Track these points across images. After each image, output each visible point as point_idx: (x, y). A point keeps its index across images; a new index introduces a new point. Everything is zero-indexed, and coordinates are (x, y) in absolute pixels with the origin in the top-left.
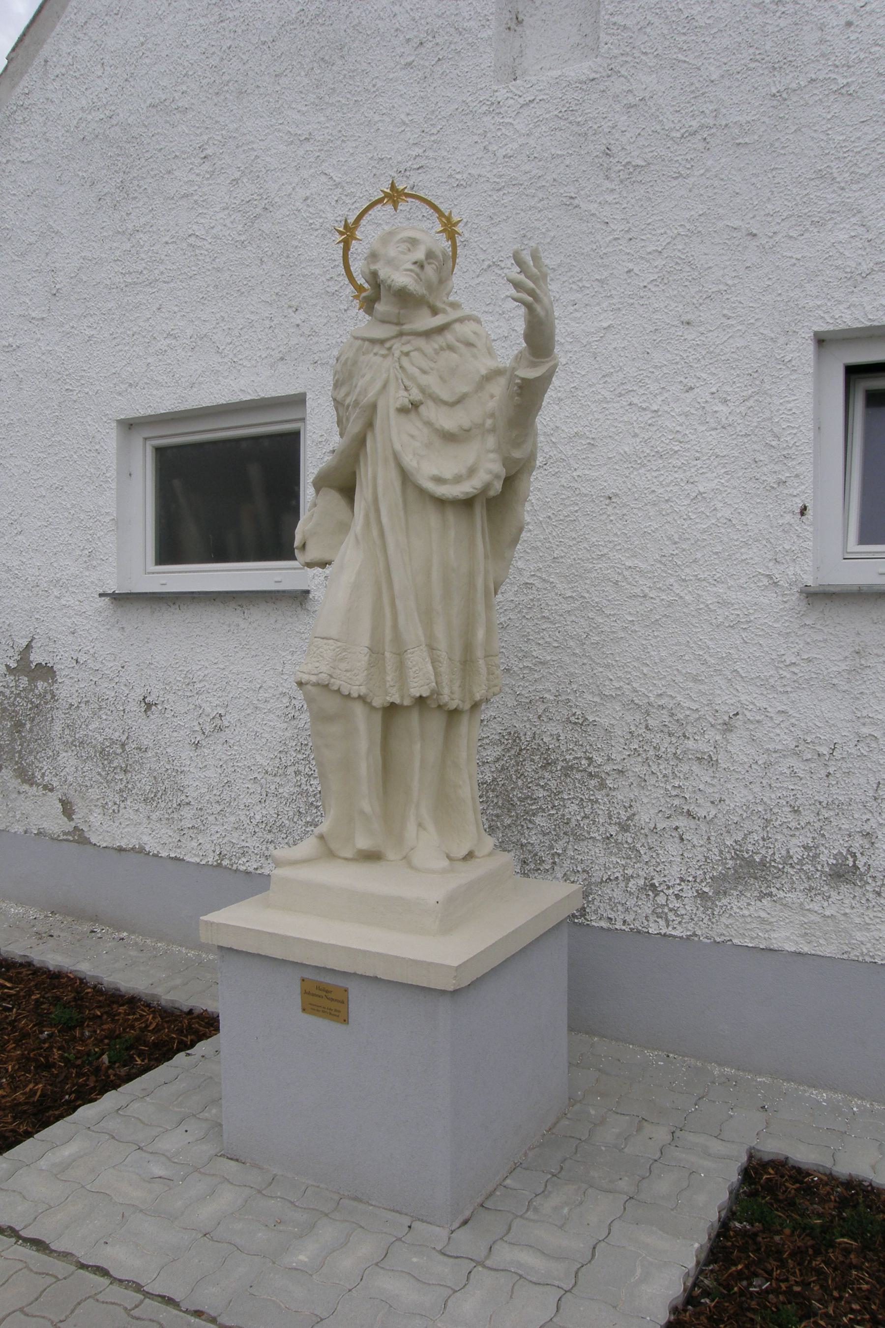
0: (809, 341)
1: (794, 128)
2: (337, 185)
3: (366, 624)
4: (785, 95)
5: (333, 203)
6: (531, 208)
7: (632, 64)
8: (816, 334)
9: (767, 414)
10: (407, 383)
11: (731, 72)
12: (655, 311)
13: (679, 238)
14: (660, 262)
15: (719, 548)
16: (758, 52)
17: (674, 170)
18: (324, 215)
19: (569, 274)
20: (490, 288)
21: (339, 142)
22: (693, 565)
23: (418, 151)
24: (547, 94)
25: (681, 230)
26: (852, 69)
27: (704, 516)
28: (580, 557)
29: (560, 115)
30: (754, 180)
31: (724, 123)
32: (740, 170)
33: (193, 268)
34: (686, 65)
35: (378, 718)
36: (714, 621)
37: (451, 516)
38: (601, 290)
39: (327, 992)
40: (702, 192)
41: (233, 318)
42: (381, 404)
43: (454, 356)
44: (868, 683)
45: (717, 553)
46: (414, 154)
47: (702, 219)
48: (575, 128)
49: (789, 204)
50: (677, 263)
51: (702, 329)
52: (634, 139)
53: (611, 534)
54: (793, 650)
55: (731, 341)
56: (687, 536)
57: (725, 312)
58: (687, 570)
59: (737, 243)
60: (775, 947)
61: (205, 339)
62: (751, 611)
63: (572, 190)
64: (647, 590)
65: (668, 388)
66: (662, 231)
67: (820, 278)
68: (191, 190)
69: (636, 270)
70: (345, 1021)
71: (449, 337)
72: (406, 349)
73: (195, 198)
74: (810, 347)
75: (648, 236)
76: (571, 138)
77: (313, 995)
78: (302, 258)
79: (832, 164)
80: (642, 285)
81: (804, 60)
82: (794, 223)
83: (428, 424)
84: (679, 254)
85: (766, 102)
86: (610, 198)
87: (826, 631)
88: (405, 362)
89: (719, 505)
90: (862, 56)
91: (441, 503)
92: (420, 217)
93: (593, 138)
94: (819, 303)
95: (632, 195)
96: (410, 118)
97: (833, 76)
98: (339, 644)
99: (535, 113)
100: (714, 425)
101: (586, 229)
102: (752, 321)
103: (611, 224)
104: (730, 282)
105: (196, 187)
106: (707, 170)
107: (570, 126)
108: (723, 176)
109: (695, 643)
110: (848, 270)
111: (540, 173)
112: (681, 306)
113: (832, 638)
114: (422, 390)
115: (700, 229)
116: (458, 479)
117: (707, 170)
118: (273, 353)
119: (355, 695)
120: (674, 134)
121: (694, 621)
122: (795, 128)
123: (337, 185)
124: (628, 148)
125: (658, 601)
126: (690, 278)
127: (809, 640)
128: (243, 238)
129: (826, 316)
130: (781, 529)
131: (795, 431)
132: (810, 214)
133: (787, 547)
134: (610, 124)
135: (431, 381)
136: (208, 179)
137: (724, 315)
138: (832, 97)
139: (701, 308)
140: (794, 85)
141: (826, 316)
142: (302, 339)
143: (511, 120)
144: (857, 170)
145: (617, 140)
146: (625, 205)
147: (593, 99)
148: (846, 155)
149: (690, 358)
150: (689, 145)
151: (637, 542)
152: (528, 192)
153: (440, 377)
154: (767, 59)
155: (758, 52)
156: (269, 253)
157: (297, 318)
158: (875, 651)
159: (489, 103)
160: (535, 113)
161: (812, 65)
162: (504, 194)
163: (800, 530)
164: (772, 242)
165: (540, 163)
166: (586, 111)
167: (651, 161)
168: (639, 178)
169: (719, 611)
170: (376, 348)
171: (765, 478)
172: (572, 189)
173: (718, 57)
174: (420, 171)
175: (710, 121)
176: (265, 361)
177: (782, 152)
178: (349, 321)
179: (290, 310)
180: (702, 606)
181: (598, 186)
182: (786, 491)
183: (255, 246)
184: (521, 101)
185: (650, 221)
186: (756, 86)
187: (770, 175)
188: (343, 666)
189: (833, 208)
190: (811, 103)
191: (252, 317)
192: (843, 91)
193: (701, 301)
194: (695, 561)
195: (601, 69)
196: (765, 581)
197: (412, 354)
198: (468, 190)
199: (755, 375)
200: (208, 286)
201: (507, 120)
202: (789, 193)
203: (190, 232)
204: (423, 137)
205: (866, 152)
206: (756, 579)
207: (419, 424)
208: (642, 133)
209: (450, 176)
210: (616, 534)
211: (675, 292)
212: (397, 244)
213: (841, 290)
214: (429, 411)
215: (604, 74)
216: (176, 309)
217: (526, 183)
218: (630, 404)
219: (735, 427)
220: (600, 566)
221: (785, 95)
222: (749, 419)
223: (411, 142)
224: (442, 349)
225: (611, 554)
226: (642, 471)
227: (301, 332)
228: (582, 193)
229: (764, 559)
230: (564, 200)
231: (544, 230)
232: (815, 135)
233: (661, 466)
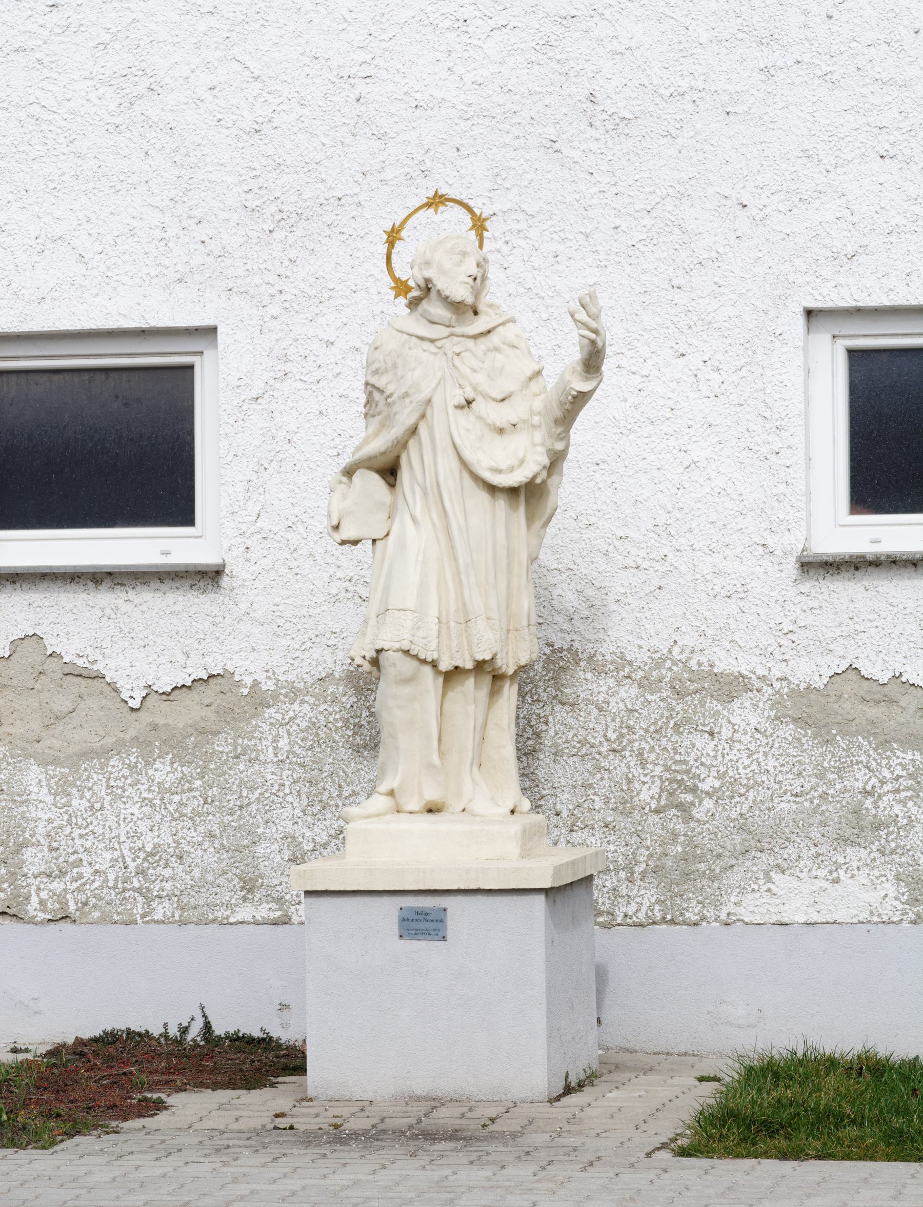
0: (799, 315)
1: (781, 104)
2: (256, 78)
3: (433, 598)
4: (772, 72)
5: (251, 99)
6: (505, 145)
7: (616, 9)
8: (805, 308)
9: (760, 386)
10: (462, 382)
11: (719, 39)
12: (644, 272)
13: (669, 199)
14: (648, 221)
15: (714, 517)
16: (745, 24)
17: (663, 128)
18: (237, 112)
19: (550, 223)
20: (457, 227)
21: (257, 26)
22: (687, 534)
23: (363, 56)
24: (522, 22)
25: (671, 191)
26: (834, 59)
27: (698, 485)
28: (566, 526)
29: (538, 48)
30: (744, 150)
31: (713, 88)
32: (730, 138)
33: (38, 147)
34: (672, 21)
35: (441, 680)
36: (711, 591)
37: (502, 503)
38: (586, 244)
39: (426, 914)
40: (691, 155)
41: (104, 221)
42: (437, 400)
43: (498, 356)
44: (862, 647)
45: (712, 523)
46: (361, 59)
47: (693, 182)
48: (554, 65)
49: (778, 179)
50: (667, 225)
51: (693, 295)
52: (620, 88)
53: (599, 502)
54: (790, 618)
55: (722, 309)
56: (681, 505)
57: (717, 280)
58: (682, 540)
59: (727, 211)
60: (786, 920)
61: (60, 242)
62: (748, 581)
63: (552, 133)
64: (639, 561)
65: (659, 352)
66: (651, 190)
67: (808, 255)
68: (30, 44)
69: (623, 227)
70: (444, 938)
71: (494, 338)
72: (457, 349)
73: (39, 55)
74: (801, 320)
75: (636, 192)
76: (550, 75)
77: (411, 920)
78: (208, 159)
79: (818, 146)
80: (630, 243)
81: (790, 41)
82: (783, 197)
83: (480, 418)
84: (669, 216)
85: (754, 75)
86: (594, 146)
87: (821, 598)
88: (457, 361)
89: (713, 474)
90: (843, 48)
91: (492, 489)
92: (369, 135)
93: (574, 80)
94: (808, 279)
95: (618, 147)
96: (354, 15)
97: (817, 62)
98: (416, 615)
99: (508, 40)
100: (706, 394)
101: (568, 176)
102: (744, 291)
103: (595, 175)
104: (721, 250)
105: (40, 43)
106: (696, 134)
107: (549, 61)
108: (713, 142)
109: (692, 613)
110: (835, 250)
111: (516, 108)
112: (671, 269)
113: (827, 604)
114: (475, 389)
115: (690, 192)
116: (511, 469)
117: (696, 134)
118: (166, 272)
119: (429, 660)
120: (662, 91)
121: (690, 592)
122: (784, 103)
123: (256, 78)
124: (614, 97)
125: (652, 570)
126: (680, 241)
127: (805, 608)
128: (118, 121)
129: (814, 292)
130: (775, 498)
131: (786, 403)
132: (798, 191)
133: (782, 517)
134: (593, 68)
135: (479, 378)
136: (58, 34)
137: (715, 283)
138: (817, 81)
139: (692, 273)
140: (780, 63)
141: (814, 292)
142: (210, 260)
143: (480, 43)
144: (842, 155)
145: (601, 87)
146: (611, 158)
147: (574, 37)
148: (831, 139)
149: (681, 324)
150: (678, 104)
151: (627, 512)
152: (502, 127)
153: (488, 376)
154: (754, 32)
155: (745, 24)
156: (158, 146)
157: (202, 233)
158: (868, 617)
159: (453, 18)
160: (508, 40)
161: (797, 47)
162: (473, 125)
163: (793, 500)
164: (762, 215)
165: (516, 97)
166: (568, 49)
167: (638, 114)
168: (626, 131)
169: (716, 581)
170: (426, 345)
171: (758, 448)
172: (552, 130)
173: (706, 20)
174: (368, 80)
175: (700, 85)
176: (155, 280)
177: (771, 126)
178: (275, 243)
179: (191, 222)
180: (698, 576)
181: (581, 132)
182: (779, 462)
183: (136, 134)
184: (492, 23)
185: (637, 177)
186: (744, 57)
187: (759, 147)
188: (420, 634)
189: (819, 188)
190: (797, 83)
191: (134, 223)
192: (827, 78)
193: (692, 266)
194: (690, 530)
195: (583, 8)
196: (761, 550)
197: (462, 354)
198: (429, 112)
199: (748, 346)
200: (63, 174)
201: (475, 42)
202: (778, 167)
203: (32, 99)
204: (370, 41)
205: (849, 139)
206: (751, 549)
207: (472, 418)
208: (628, 84)
209: (407, 93)
210: (605, 502)
211: (665, 255)
212: (437, 247)
213: (828, 268)
214: (479, 406)
215: (587, 13)
216: (11, 197)
217: (499, 117)
218: (619, 367)
219: (728, 397)
220: (588, 536)
221: (772, 72)
222: (742, 389)
223: (355, 44)
224: (489, 350)
225: (600, 524)
226: (632, 436)
227: (207, 251)
228: (564, 137)
229: (759, 528)
230: (544, 141)
231: (520, 172)
232: (800, 114)
233: (652, 432)
